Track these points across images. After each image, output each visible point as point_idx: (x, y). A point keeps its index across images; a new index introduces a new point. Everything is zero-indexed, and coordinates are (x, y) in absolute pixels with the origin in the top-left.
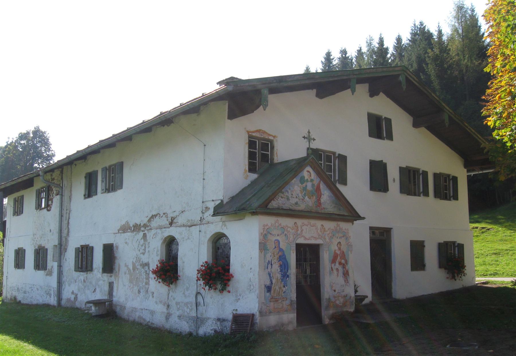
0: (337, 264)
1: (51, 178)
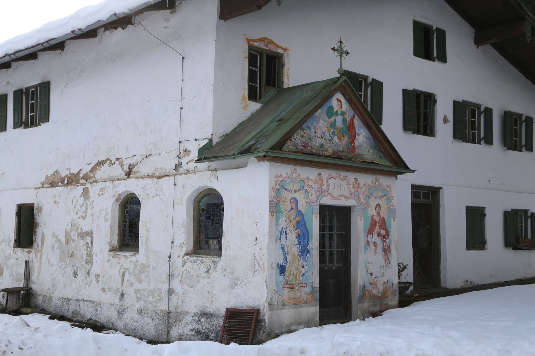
0: (375, 235)
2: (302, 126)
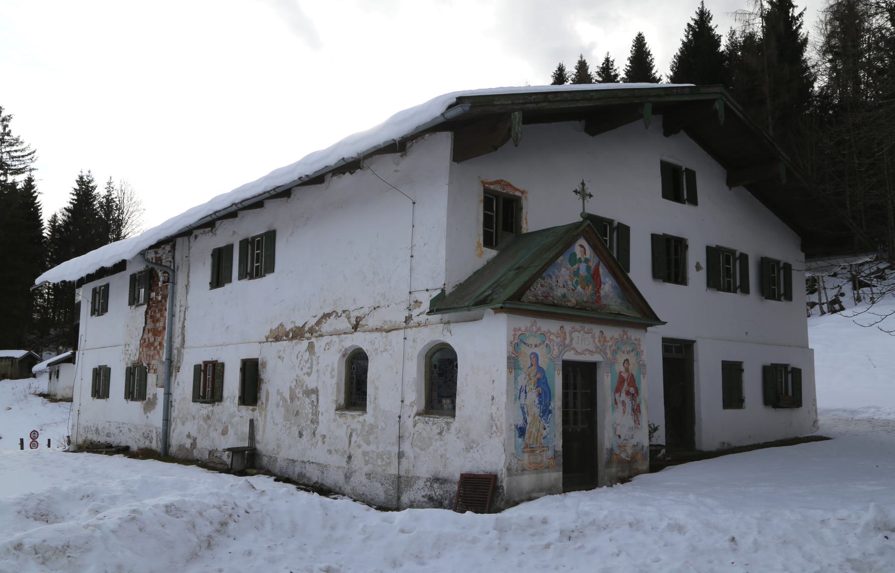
1: (156, 257)
2: (542, 275)
